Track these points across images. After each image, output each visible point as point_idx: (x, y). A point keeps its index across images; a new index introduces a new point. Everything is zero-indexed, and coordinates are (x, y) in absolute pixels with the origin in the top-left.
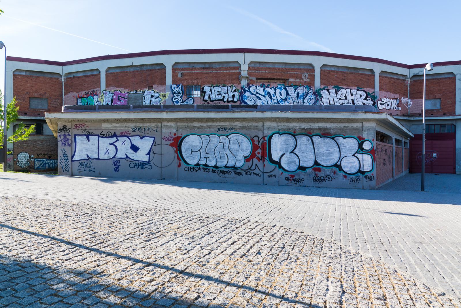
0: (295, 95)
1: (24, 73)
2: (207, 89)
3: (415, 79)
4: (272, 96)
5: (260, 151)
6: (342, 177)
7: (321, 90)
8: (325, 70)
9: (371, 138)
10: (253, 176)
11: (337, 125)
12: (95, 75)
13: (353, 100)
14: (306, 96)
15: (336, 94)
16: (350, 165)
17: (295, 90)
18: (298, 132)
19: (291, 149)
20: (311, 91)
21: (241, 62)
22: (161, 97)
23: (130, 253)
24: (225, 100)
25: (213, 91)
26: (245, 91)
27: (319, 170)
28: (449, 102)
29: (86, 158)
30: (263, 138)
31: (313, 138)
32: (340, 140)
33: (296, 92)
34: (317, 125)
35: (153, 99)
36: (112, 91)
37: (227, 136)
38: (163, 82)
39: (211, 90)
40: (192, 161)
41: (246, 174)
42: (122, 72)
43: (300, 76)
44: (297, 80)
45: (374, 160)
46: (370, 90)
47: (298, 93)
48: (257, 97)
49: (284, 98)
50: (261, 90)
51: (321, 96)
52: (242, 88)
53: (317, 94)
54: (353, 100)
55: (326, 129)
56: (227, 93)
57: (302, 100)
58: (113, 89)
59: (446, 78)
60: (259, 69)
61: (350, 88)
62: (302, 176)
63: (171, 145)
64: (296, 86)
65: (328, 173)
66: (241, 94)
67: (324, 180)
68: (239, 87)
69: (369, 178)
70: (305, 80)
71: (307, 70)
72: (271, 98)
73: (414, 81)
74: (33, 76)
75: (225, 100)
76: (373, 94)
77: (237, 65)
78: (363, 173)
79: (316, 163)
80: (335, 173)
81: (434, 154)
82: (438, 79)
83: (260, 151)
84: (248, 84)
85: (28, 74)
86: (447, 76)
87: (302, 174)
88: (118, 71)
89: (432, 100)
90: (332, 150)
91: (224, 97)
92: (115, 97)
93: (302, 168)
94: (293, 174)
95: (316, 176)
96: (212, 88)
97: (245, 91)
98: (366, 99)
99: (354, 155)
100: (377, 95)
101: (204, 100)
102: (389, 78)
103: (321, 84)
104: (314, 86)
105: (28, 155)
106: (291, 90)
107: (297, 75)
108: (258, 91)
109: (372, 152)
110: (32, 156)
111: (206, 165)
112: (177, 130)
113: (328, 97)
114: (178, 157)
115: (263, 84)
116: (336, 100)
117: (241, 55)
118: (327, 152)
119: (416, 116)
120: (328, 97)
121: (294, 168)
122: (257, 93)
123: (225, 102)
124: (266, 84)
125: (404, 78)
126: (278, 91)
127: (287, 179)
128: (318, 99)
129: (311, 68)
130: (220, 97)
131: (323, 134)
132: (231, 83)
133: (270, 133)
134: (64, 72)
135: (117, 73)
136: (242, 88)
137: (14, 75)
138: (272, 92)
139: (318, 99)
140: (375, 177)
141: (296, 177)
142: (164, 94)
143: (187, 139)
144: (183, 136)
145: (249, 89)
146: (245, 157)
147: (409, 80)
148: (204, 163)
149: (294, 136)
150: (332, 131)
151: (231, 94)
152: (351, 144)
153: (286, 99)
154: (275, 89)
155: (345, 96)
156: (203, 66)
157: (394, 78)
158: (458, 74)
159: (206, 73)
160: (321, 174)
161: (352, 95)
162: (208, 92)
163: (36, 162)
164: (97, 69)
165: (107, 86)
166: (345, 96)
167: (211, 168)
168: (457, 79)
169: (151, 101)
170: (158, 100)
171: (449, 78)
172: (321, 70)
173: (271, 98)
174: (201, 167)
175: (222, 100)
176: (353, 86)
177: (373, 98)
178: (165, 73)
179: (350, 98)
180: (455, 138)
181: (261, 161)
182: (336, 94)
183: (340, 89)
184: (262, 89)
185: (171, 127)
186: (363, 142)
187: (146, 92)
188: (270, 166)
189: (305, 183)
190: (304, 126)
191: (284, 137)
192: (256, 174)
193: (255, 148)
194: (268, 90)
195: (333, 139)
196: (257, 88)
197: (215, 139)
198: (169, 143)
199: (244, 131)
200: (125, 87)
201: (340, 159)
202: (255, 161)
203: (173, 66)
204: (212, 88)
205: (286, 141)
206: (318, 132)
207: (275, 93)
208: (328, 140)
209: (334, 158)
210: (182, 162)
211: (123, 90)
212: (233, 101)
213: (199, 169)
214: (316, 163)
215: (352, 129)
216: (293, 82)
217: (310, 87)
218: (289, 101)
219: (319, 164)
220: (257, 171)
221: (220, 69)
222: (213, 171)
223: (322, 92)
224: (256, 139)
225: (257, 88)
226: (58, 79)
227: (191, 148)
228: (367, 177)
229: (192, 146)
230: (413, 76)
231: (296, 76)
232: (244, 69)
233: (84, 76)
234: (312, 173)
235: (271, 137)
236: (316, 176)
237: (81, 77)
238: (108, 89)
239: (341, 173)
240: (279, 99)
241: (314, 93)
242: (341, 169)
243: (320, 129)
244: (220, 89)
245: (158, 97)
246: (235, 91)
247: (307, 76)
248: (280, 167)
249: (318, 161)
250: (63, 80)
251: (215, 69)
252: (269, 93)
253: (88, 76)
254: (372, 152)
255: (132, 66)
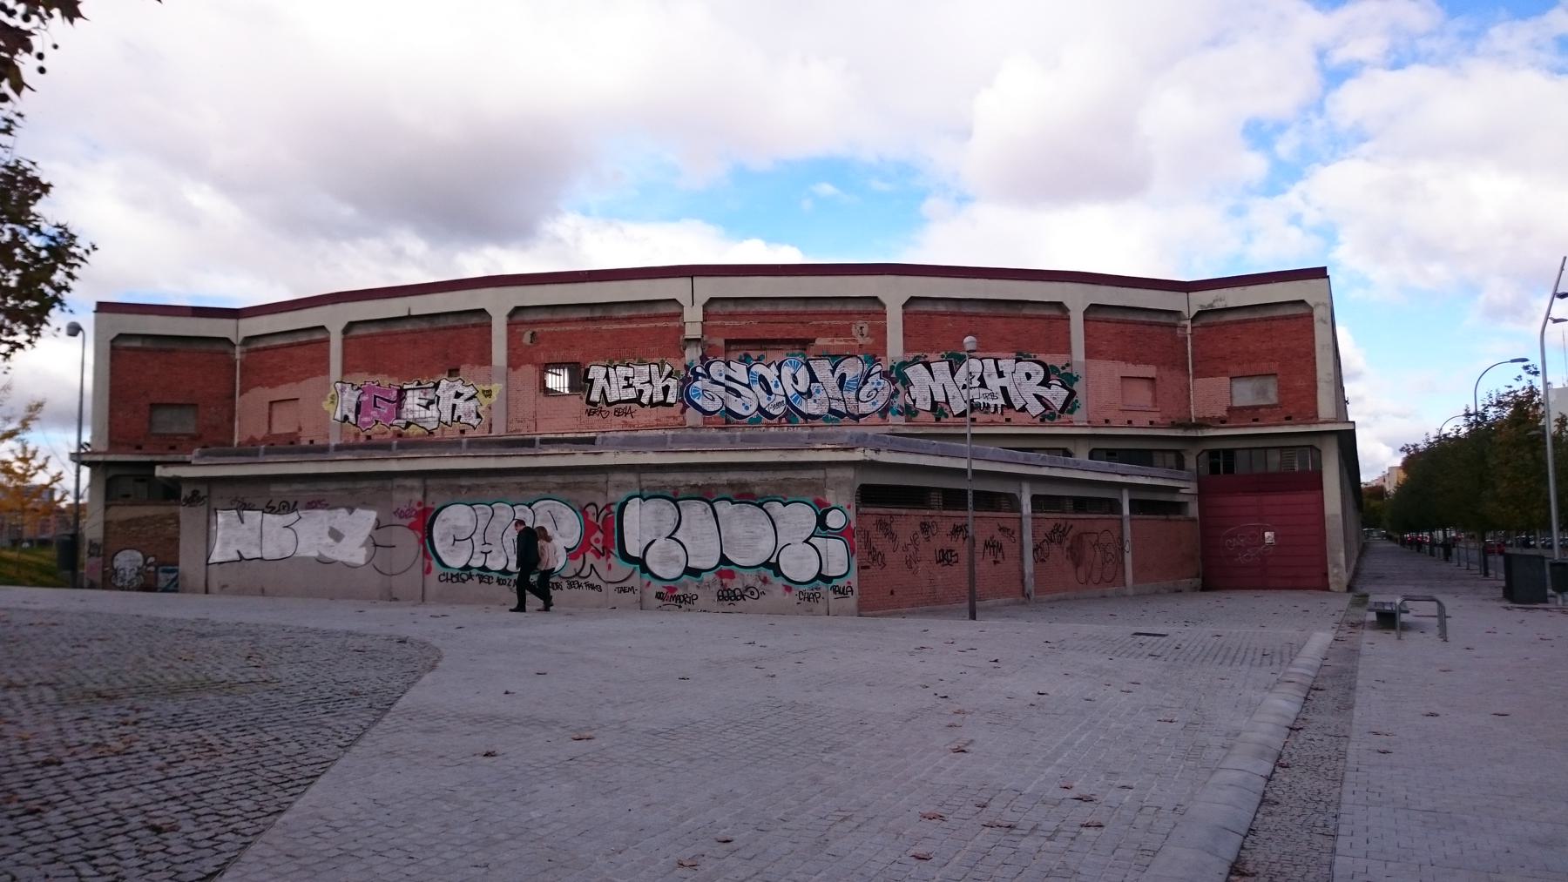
0: (833, 381)
1: (137, 344)
2: (597, 373)
3: (1205, 320)
4: (772, 385)
5: (599, 535)
6: (781, 590)
7: (905, 364)
8: (916, 313)
9: (843, 503)
10: (584, 591)
11: (768, 476)
12: (316, 338)
13: (1004, 390)
14: (865, 382)
15: (953, 374)
16: (799, 564)
17: (835, 368)
18: (682, 492)
19: (669, 530)
20: (878, 368)
21: (684, 299)
22: (480, 396)
23: (203, 636)
24: (645, 400)
25: (613, 380)
26: (696, 375)
27: (731, 575)
28: (1300, 383)
29: (236, 557)
30: (607, 506)
31: (718, 506)
32: (776, 508)
33: (837, 374)
34: (724, 478)
35: (459, 402)
36: (359, 384)
37: (530, 506)
38: (485, 358)
39: (607, 376)
40: (456, 561)
41: (571, 586)
42: (383, 335)
43: (845, 332)
44: (839, 343)
45: (851, 551)
46: (1055, 360)
47: (843, 376)
48: (728, 389)
49: (804, 390)
50: (740, 372)
51: (907, 382)
52: (687, 367)
53: (897, 375)
54: (1004, 390)
55: (745, 485)
56: (650, 382)
57: (853, 394)
58: (360, 378)
59: (1287, 318)
60: (731, 316)
61: (995, 355)
62: (692, 590)
63: (411, 527)
64: (836, 359)
65: (750, 581)
66: (685, 384)
67: (742, 596)
68: (680, 367)
69: (842, 592)
70: (861, 341)
71: (865, 315)
72: (769, 392)
73: (1204, 326)
74: (160, 350)
75: (645, 400)
76: (1068, 370)
77: (673, 309)
78: (828, 580)
79: (724, 560)
80: (765, 581)
81: (1267, 534)
82: (1266, 320)
83: (599, 535)
84: (703, 358)
85: (148, 344)
86: (1289, 311)
87: (691, 583)
88: (374, 330)
89: (1255, 380)
90: (758, 531)
91: (641, 392)
92: (364, 398)
93: (691, 571)
94: (672, 584)
95: (724, 588)
96: (611, 370)
97: (696, 375)
98: (1045, 383)
99: (806, 541)
100: (1077, 370)
101: (589, 402)
102: (1118, 322)
103: (907, 349)
104: (885, 354)
105: (139, 555)
106: (822, 369)
107: (838, 327)
108: (732, 374)
109: (845, 533)
110: (151, 560)
111: (484, 568)
112: (425, 496)
113: (926, 384)
114: (425, 551)
115: (747, 355)
116: (952, 391)
117: (686, 282)
118: (748, 535)
119: (1209, 427)
120: (926, 384)
121: (675, 571)
122: (728, 378)
123: (643, 405)
124: (754, 355)
125: (1173, 320)
126: (787, 371)
127: (659, 596)
128: (897, 391)
129: (877, 308)
130: (631, 394)
131: (738, 496)
132: (660, 355)
133: (622, 497)
134: (242, 335)
135: (371, 335)
136: (687, 367)
137: (113, 348)
138: (771, 374)
139: (897, 391)
140: (856, 590)
141: (680, 592)
142: (486, 388)
143: (444, 514)
144: (437, 507)
145: (707, 369)
146: (568, 550)
147: (1188, 323)
148: (480, 564)
149: (675, 501)
150: (757, 490)
151: (659, 384)
152: (800, 517)
153: (809, 394)
154: (779, 368)
155: (981, 379)
156: (586, 314)
157: (1135, 323)
158: (1317, 305)
159: (595, 332)
160: (735, 584)
161: (1001, 374)
162: (600, 382)
163: (161, 575)
164: (322, 328)
165: (346, 370)
166: (981, 379)
167: (496, 576)
168: (1316, 318)
169: (454, 406)
170: (472, 404)
171: (1296, 317)
172: (905, 314)
173: (769, 392)
174: (474, 572)
175: (637, 400)
176: (1006, 350)
177: (1068, 381)
178: (490, 333)
179: (994, 383)
180: (1321, 487)
181: (603, 559)
182: (953, 374)
183: (962, 359)
184: (743, 368)
185: (412, 489)
186: (826, 513)
187: (444, 383)
188: (621, 569)
189: (700, 603)
190: (697, 479)
191: (652, 505)
192: (592, 587)
193: (588, 529)
194: (759, 369)
195: (760, 506)
196: (728, 365)
197: (504, 513)
198: (407, 522)
199: (565, 494)
200: (391, 373)
201: (777, 551)
202: (590, 558)
203: (510, 315)
204: (611, 370)
205: (658, 513)
206: (727, 493)
207: (779, 377)
208: (749, 510)
209: (764, 549)
210: (434, 563)
211: (385, 381)
212: (664, 403)
213: (470, 576)
214: (724, 560)
215: (802, 484)
216: (828, 347)
217: (873, 360)
218: (818, 396)
219: (731, 563)
220: (593, 580)
221: (630, 319)
222: (498, 580)
223: (909, 371)
224: (591, 509)
225: (728, 365)
226: (225, 353)
227: (453, 532)
228: (835, 590)
229: (456, 527)
230: (1199, 313)
231: (837, 332)
232: (693, 320)
233: (291, 345)
234: (714, 582)
235: (623, 506)
236: (724, 588)
237: (282, 346)
238: (348, 378)
239: (780, 581)
240: (791, 392)
241: (885, 375)
242: (777, 571)
243: (731, 485)
244: (630, 372)
245: (473, 397)
246: (669, 375)
247: (865, 330)
248: (645, 569)
249: (730, 557)
250: (238, 356)
251: (618, 320)
252: (762, 378)
253: (300, 344)
254: (845, 533)
255: (409, 317)
